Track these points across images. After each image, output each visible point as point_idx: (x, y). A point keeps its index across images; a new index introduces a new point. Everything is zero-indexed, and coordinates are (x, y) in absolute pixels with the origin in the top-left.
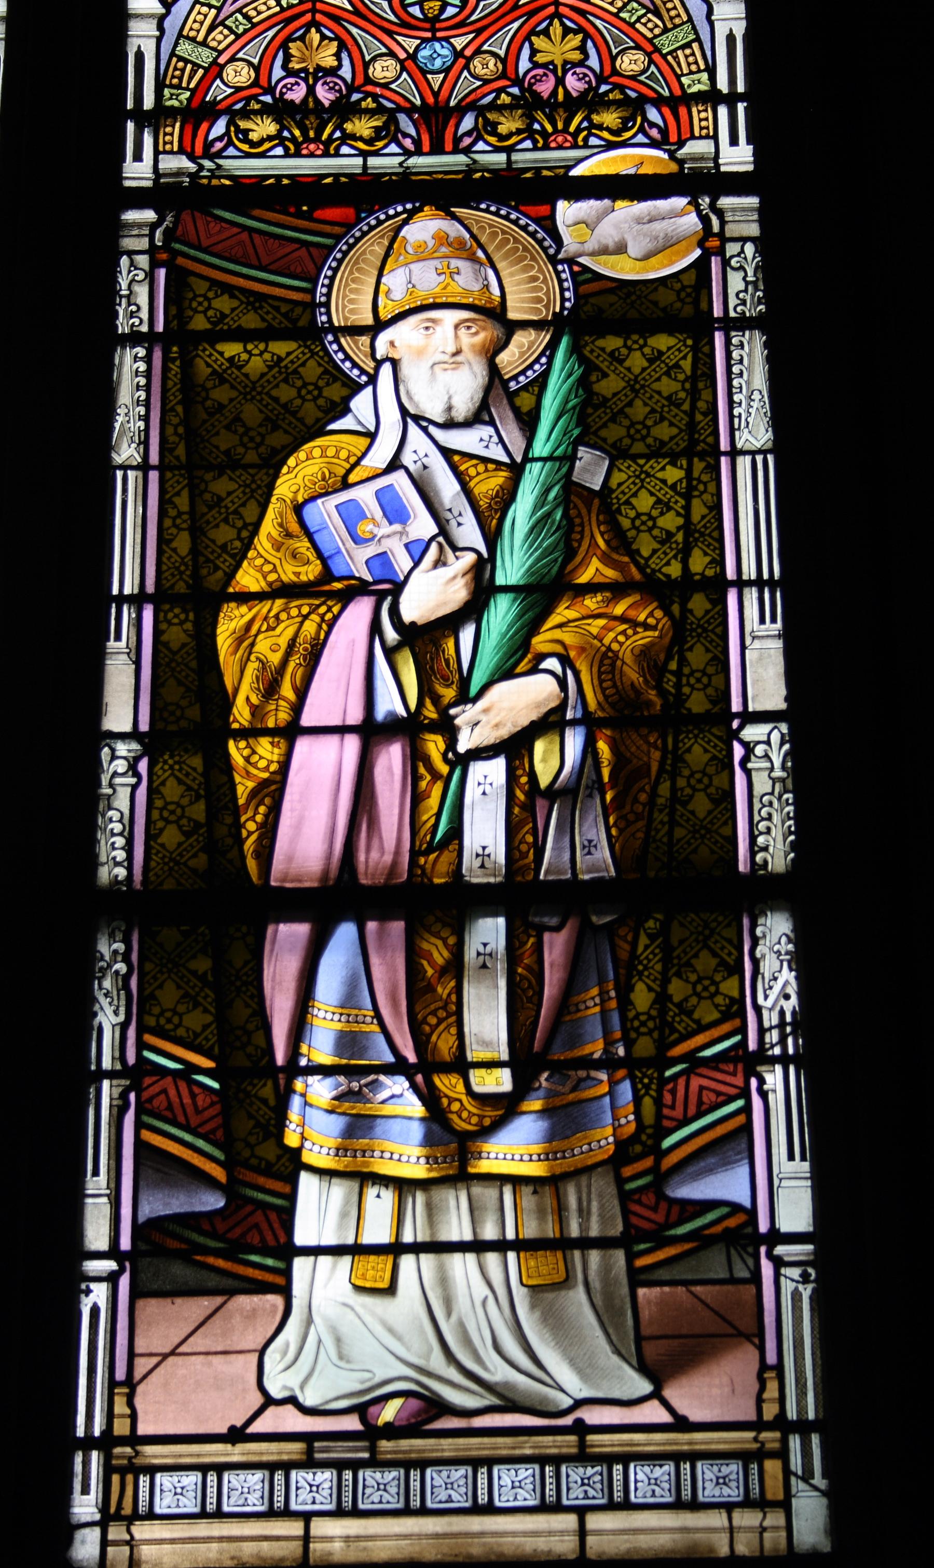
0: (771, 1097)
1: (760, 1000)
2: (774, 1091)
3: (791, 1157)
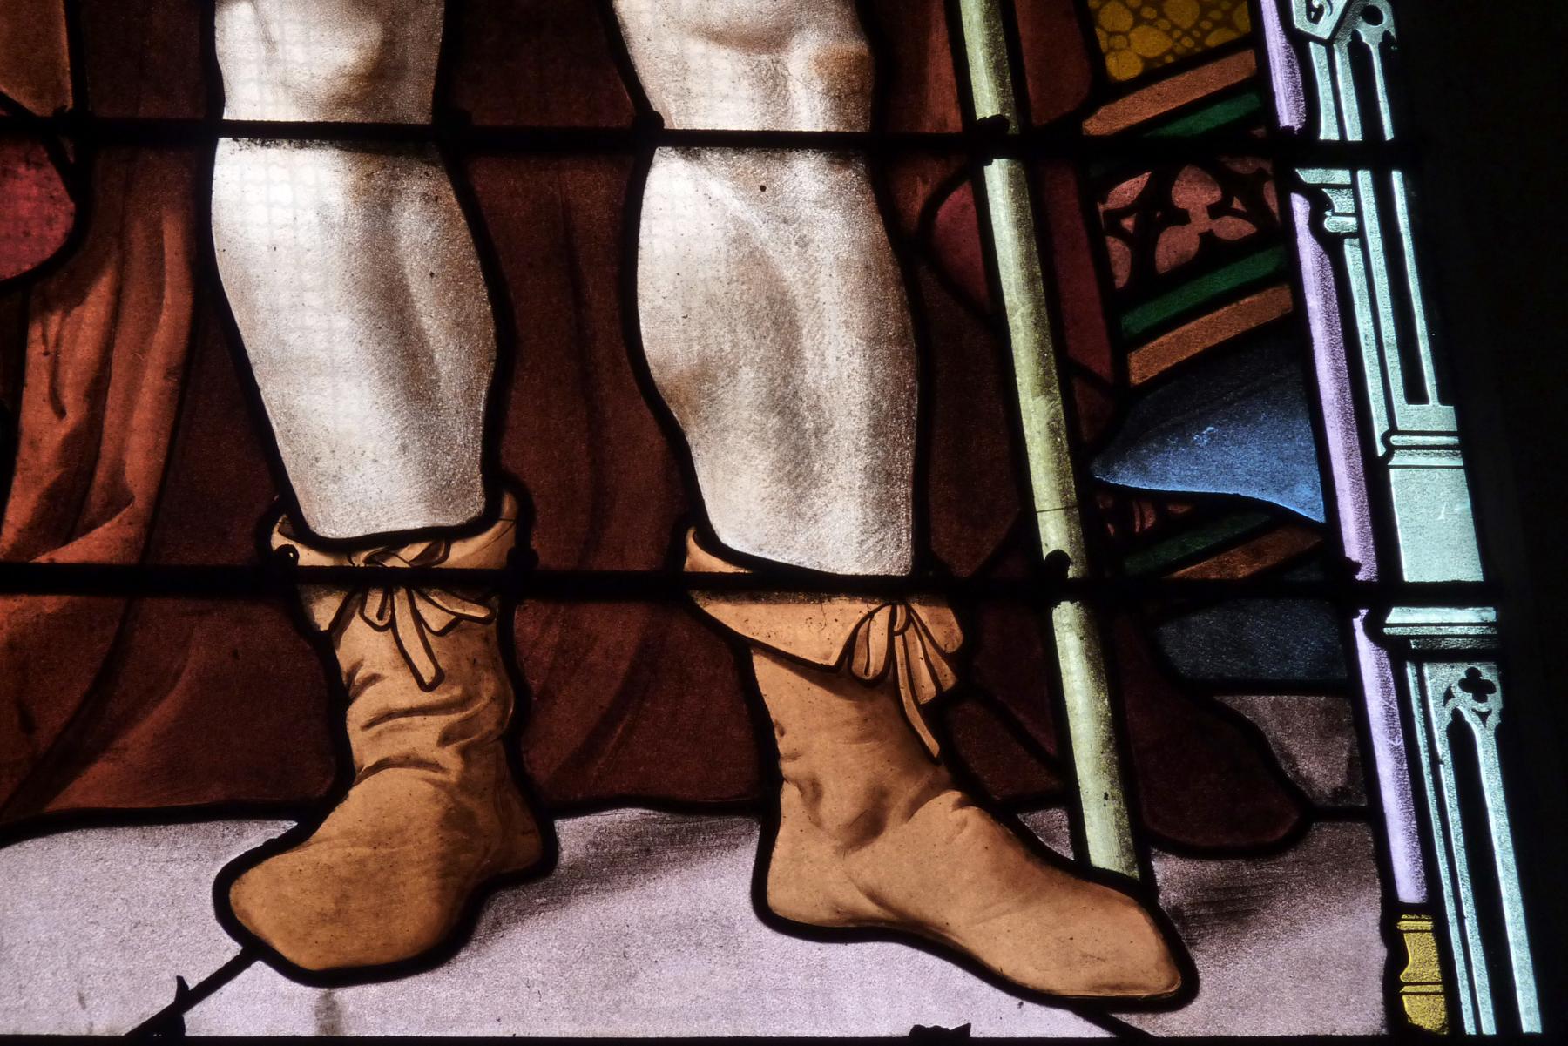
0: (1351, 253)
1: (1300, 21)
2: (1360, 233)
3: (1415, 393)
